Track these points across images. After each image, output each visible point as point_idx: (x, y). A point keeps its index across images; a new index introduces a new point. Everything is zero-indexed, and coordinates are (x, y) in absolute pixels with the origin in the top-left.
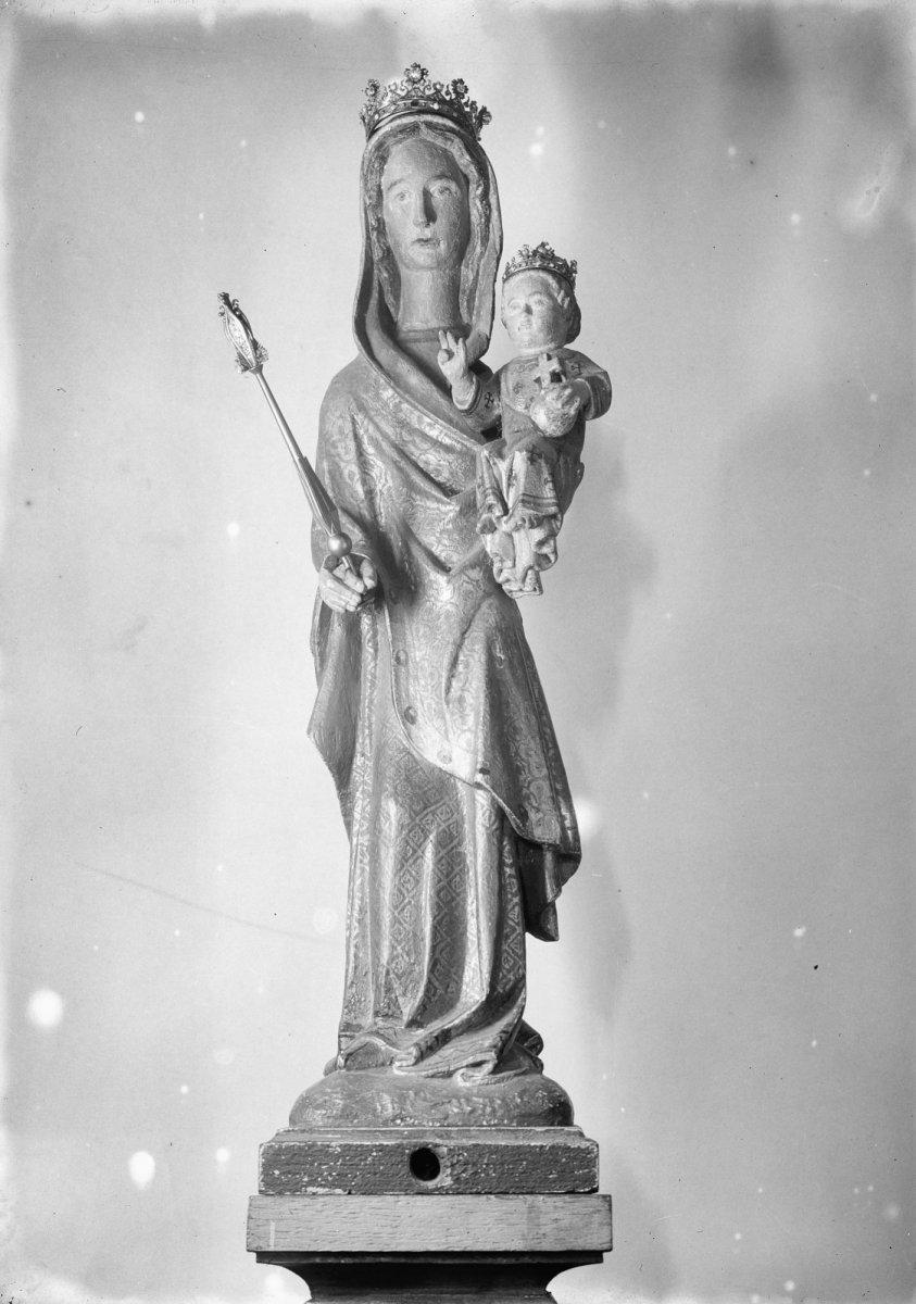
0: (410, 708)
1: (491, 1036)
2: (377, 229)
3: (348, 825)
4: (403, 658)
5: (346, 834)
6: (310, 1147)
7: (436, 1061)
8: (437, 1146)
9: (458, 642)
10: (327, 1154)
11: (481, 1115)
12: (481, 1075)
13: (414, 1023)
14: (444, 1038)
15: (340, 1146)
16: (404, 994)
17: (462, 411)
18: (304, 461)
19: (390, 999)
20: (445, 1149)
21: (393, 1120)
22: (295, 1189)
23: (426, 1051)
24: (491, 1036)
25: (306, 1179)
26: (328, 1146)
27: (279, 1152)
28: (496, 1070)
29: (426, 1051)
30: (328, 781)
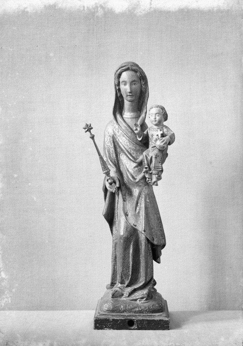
0: (127, 212)
1: (145, 292)
2: (118, 91)
3: (112, 233)
4: (125, 200)
5: (109, 229)
6: (105, 319)
7: (133, 297)
8: (134, 319)
9: (140, 210)
10: (109, 321)
11: (143, 311)
12: (143, 301)
13: (128, 286)
14: (135, 290)
15: (112, 319)
16: (125, 279)
17: (139, 141)
18: (101, 158)
19: (122, 280)
20: (136, 320)
21: (124, 312)
22: (102, 328)
23: (131, 294)
24: (145, 292)
25: (104, 327)
26: (109, 319)
27: (98, 320)
28: (146, 300)
29: (131, 294)
30: (107, 225)
